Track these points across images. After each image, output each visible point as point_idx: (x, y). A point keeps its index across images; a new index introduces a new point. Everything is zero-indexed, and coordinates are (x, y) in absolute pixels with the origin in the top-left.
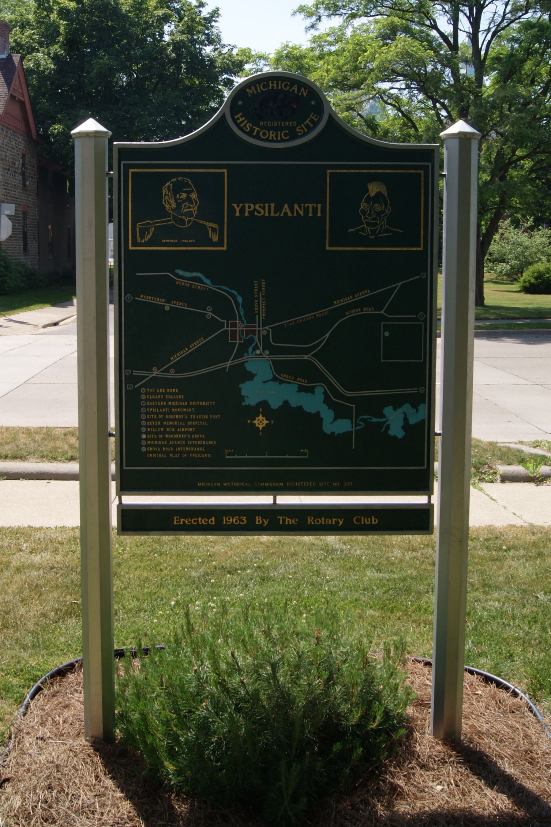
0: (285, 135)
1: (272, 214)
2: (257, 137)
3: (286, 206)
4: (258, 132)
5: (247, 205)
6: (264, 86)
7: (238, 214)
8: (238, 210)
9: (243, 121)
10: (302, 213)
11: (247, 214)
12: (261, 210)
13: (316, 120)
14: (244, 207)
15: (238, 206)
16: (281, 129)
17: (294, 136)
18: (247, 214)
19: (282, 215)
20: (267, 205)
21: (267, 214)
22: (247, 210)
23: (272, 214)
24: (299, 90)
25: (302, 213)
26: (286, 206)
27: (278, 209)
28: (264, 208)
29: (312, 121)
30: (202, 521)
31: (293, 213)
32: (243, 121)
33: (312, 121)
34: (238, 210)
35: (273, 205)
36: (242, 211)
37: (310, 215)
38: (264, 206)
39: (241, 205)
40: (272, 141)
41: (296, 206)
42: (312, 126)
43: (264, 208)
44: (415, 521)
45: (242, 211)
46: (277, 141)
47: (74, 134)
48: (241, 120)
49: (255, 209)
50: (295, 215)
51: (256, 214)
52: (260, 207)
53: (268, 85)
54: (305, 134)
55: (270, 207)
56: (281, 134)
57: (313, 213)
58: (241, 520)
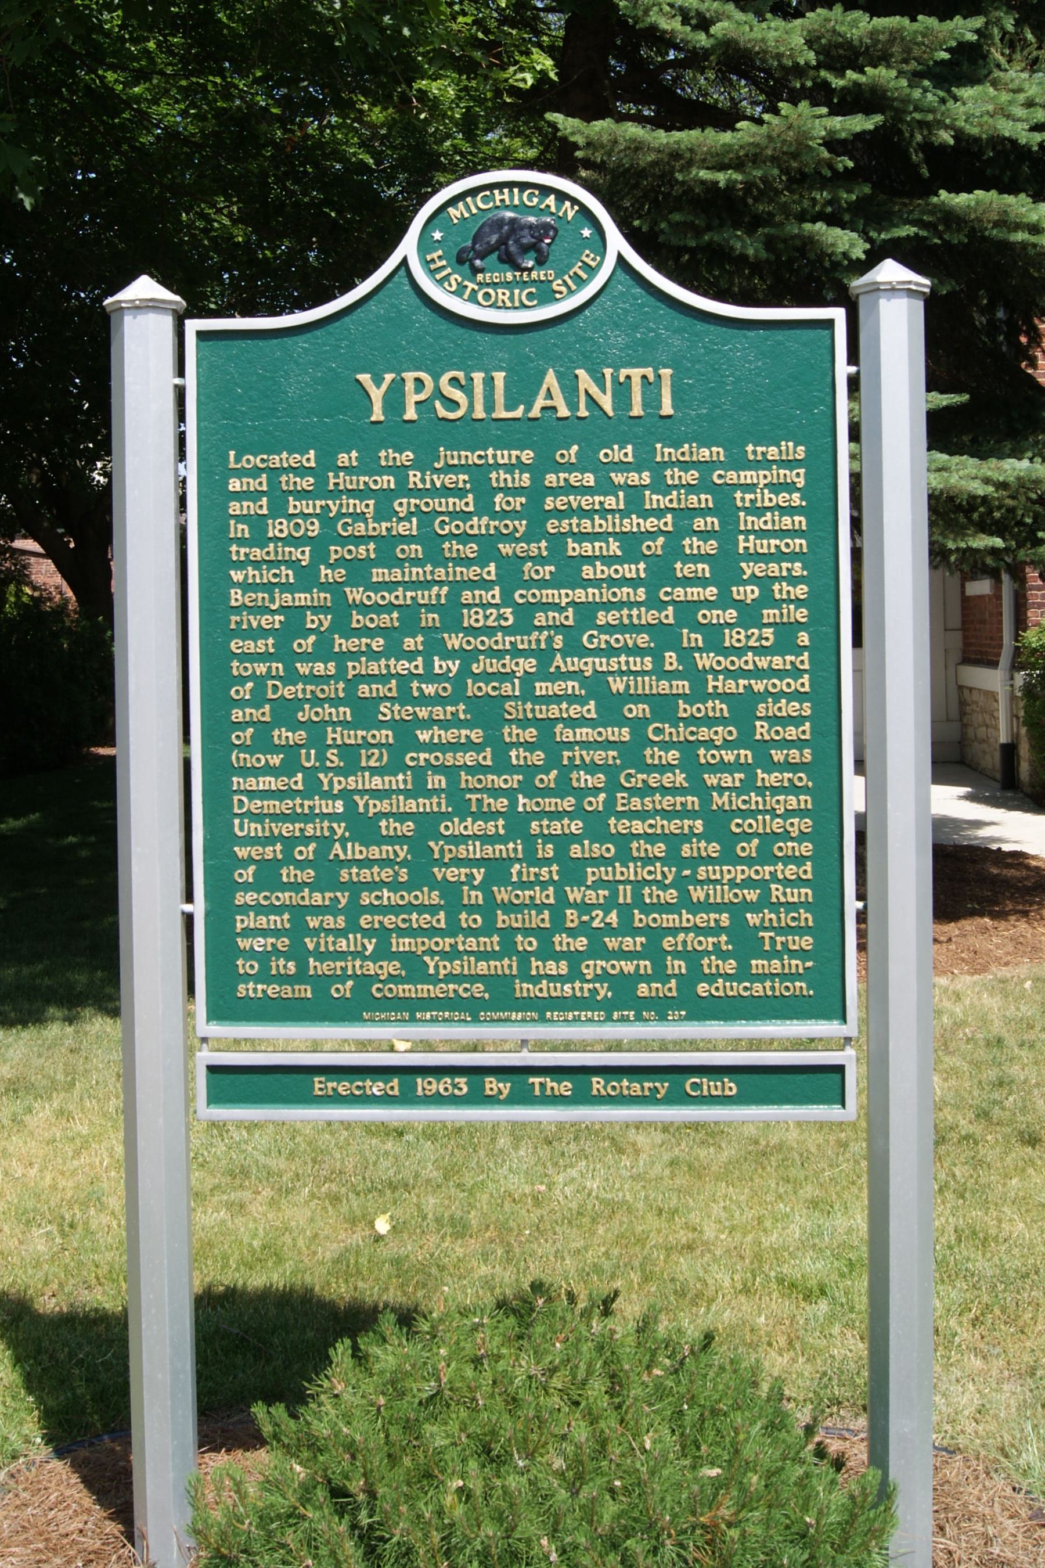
3: (551, 379)
5: (409, 376)
7: (377, 415)
8: (377, 394)
9: (443, 267)
10: (606, 402)
11: (411, 414)
12: (458, 395)
13: (593, 264)
14: (399, 384)
15: (378, 381)
17: (547, 296)
20: (478, 377)
21: (479, 413)
25: (606, 402)
26: (551, 379)
28: (467, 389)
31: (573, 406)
32: (443, 267)
34: (377, 394)
36: (395, 399)
42: (585, 276)
43: (467, 389)
44: (823, 1081)
45: (395, 399)
47: (1034, 773)
52: (454, 381)
57: (645, 405)
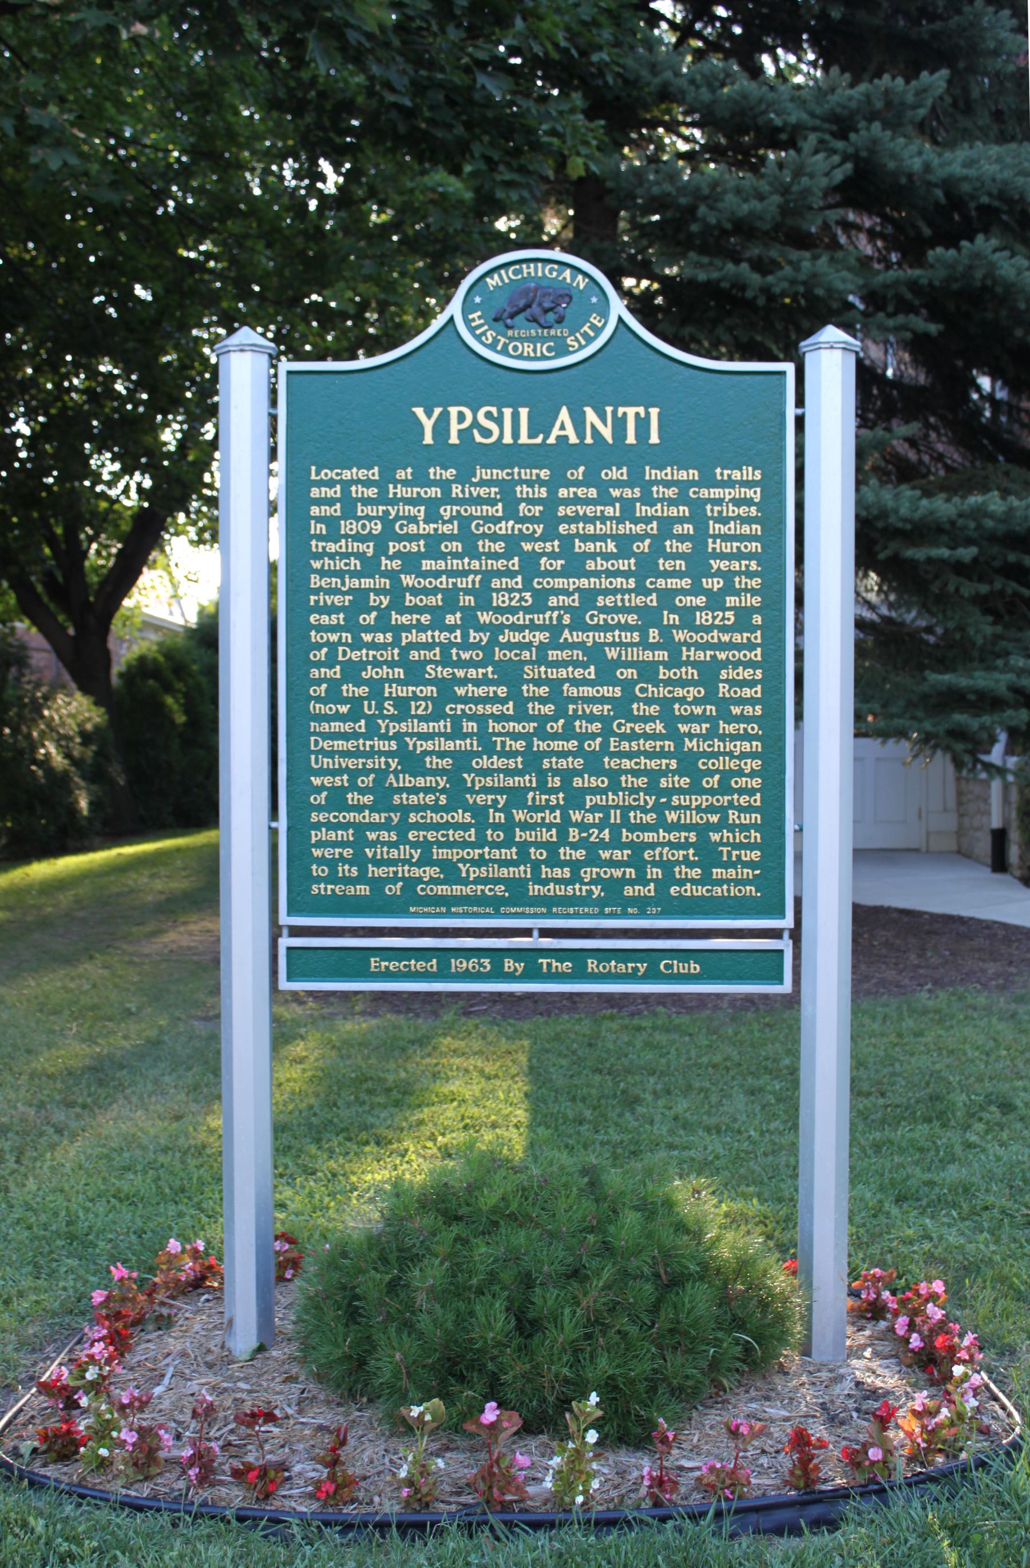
0: (549, 349)
1: (524, 439)
2: (504, 352)
3: (564, 415)
4: (506, 345)
5: (454, 411)
6: (515, 273)
7: (428, 439)
8: (428, 424)
10: (607, 433)
11: (454, 439)
14: (445, 417)
15: (429, 414)
16: (543, 340)
17: (562, 350)
18: (454, 439)
19: (552, 440)
20: (508, 412)
21: (508, 439)
22: (454, 427)
23: (524, 439)
24: (573, 279)
25: (607, 433)
26: (564, 415)
27: (541, 424)
28: (499, 421)
29: (593, 327)
30: (419, 965)
33: (593, 327)
34: (428, 424)
35: (524, 412)
36: (442, 427)
37: (631, 439)
38: (501, 414)
39: (438, 411)
40: (529, 358)
41: (591, 416)
43: (499, 421)
45: (442, 427)
46: (536, 359)
48: (478, 322)
49: (475, 424)
50: (589, 440)
51: (478, 438)
52: (488, 415)
53: (520, 271)
54: (581, 347)
55: (516, 417)
56: (542, 349)
58: (481, 965)
